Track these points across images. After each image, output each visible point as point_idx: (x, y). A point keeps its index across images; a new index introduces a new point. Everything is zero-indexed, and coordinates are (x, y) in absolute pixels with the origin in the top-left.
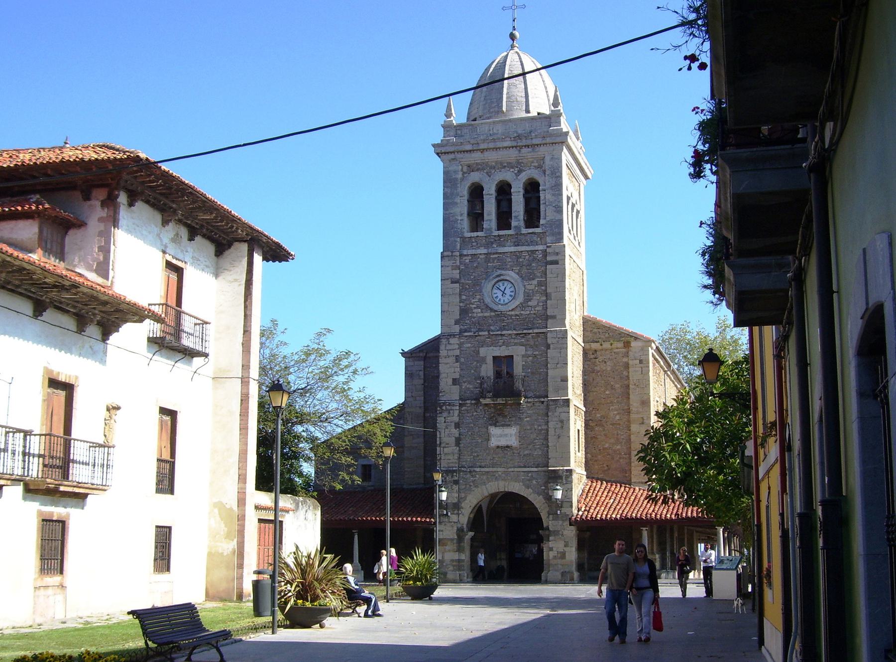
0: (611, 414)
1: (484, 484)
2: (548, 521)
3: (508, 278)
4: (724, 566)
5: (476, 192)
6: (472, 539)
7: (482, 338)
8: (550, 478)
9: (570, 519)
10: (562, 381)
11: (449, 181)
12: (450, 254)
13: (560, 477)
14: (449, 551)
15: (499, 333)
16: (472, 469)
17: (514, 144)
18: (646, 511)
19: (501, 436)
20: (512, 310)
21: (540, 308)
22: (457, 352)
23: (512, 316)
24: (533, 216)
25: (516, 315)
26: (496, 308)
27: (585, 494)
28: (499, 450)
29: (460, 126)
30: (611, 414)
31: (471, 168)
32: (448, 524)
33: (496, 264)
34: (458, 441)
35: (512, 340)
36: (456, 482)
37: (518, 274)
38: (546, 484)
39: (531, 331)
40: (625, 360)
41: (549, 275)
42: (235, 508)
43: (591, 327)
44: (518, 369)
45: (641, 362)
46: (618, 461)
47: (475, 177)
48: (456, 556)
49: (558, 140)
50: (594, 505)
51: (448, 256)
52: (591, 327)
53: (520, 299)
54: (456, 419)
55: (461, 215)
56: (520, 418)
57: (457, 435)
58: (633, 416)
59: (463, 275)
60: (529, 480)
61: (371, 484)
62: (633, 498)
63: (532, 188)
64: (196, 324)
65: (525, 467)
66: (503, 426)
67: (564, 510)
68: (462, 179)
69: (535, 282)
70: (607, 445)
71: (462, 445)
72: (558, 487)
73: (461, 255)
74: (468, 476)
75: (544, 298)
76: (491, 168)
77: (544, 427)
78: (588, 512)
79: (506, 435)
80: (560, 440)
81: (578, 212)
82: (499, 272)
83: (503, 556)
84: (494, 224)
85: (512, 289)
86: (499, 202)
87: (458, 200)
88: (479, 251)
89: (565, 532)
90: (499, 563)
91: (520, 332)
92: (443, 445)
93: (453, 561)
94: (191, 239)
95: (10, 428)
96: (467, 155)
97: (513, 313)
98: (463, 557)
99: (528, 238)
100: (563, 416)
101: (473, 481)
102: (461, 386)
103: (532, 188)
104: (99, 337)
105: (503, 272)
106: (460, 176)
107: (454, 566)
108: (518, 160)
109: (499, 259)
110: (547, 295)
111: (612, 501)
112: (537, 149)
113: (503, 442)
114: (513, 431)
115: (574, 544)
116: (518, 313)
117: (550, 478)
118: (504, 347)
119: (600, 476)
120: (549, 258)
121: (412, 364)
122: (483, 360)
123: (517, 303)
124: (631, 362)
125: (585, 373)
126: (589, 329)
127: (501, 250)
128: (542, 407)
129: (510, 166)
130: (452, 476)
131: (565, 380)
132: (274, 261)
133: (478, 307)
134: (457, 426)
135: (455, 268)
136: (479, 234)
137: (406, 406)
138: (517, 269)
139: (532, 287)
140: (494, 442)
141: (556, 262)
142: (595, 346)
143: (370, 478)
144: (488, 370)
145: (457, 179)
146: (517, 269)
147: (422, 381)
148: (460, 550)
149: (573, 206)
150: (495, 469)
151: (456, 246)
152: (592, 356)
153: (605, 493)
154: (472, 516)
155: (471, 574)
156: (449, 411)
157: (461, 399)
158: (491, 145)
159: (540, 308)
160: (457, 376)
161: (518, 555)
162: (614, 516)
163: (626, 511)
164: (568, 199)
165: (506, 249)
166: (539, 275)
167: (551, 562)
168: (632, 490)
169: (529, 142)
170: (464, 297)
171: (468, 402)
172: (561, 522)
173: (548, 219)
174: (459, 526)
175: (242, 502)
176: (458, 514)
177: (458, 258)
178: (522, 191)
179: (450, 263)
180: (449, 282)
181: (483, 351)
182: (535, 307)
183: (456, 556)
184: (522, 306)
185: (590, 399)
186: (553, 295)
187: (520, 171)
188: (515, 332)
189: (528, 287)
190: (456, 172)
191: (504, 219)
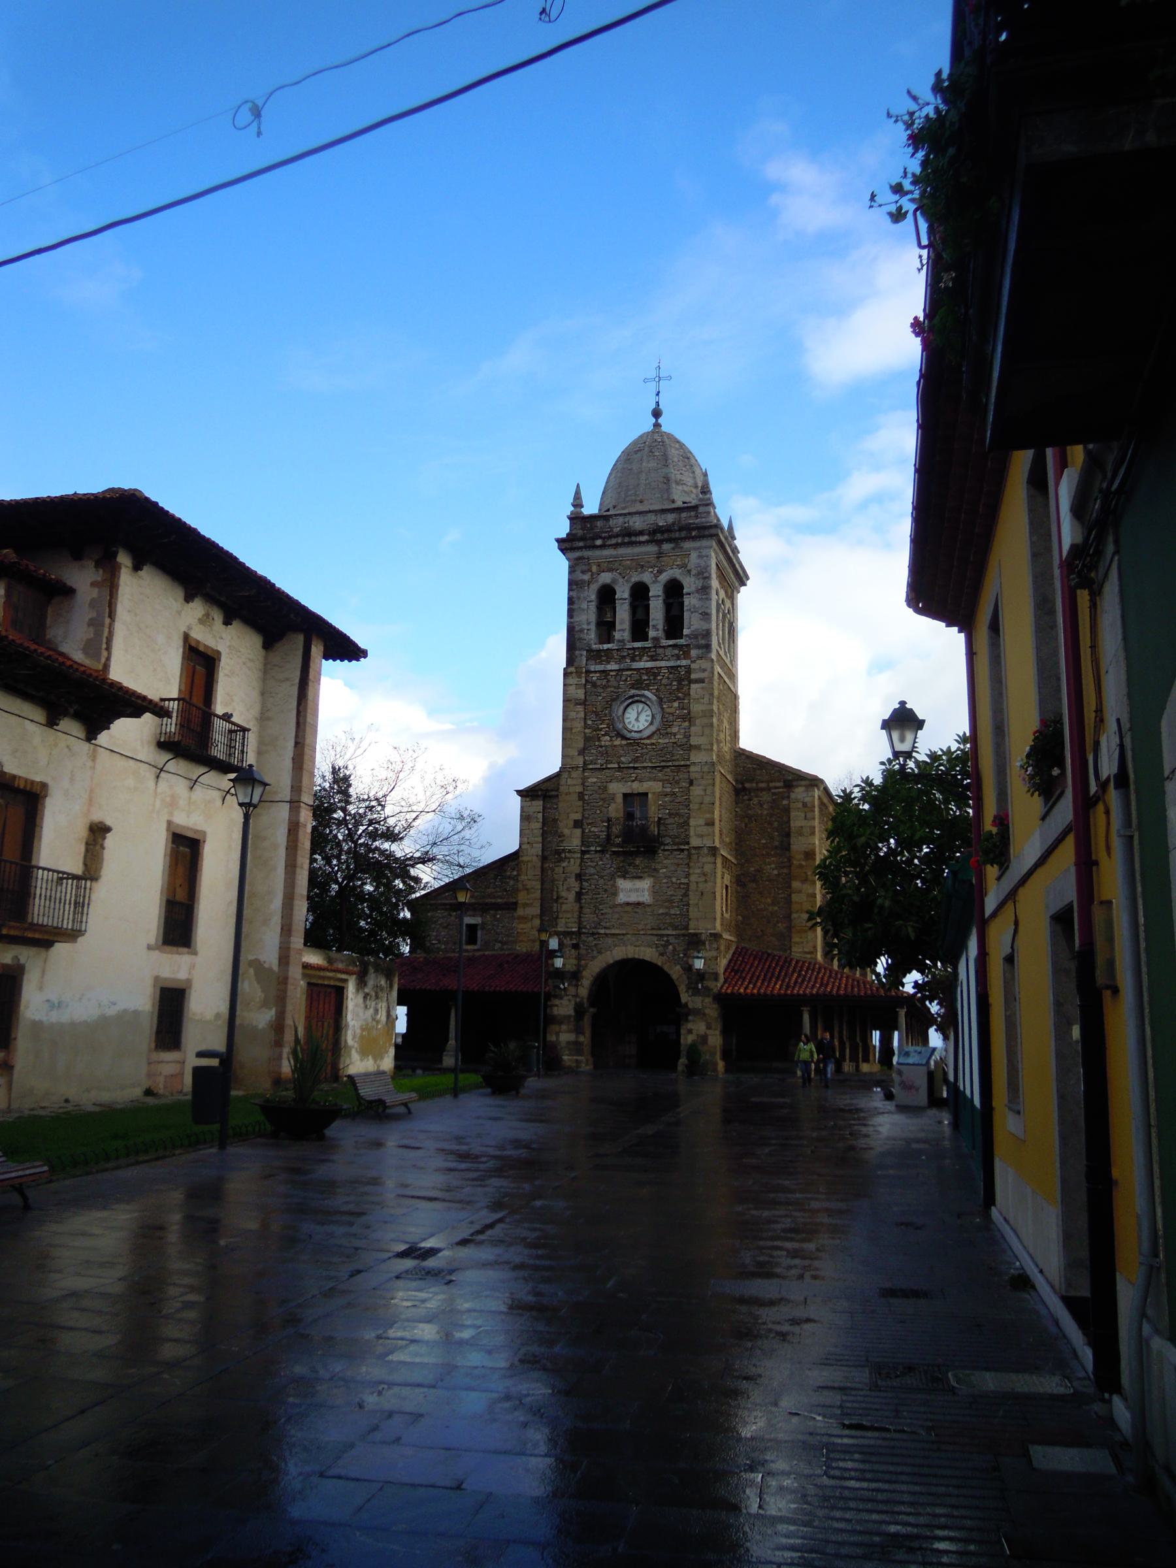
4: (910, 1061)
19: (631, 890)
20: (648, 738)
26: (629, 735)
28: (629, 908)
29: (592, 518)
34: (579, 895)
42: (275, 968)
44: (654, 812)
47: (606, 578)
48: (571, 1037)
55: (589, 624)
63: (674, 590)
64: (231, 731)
79: (637, 890)
82: (633, 692)
84: (627, 635)
86: (634, 609)
88: (609, 667)
93: (568, 1043)
94: (227, 622)
95: (64, 873)
98: (581, 1039)
103: (674, 590)
104: (82, 735)
113: (633, 898)
114: (646, 884)
120: (693, 676)
127: (636, 665)
132: (342, 660)
140: (622, 898)
141: (702, 681)
144: (616, 810)
147: (539, 825)
148: (578, 1031)
149: (724, 616)
160: (578, 817)
162: (808, 991)
164: (718, 605)
165: (641, 665)
175: (284, 957)
183: (571, 1037)
187: (660, 572)
191: (639, 629)
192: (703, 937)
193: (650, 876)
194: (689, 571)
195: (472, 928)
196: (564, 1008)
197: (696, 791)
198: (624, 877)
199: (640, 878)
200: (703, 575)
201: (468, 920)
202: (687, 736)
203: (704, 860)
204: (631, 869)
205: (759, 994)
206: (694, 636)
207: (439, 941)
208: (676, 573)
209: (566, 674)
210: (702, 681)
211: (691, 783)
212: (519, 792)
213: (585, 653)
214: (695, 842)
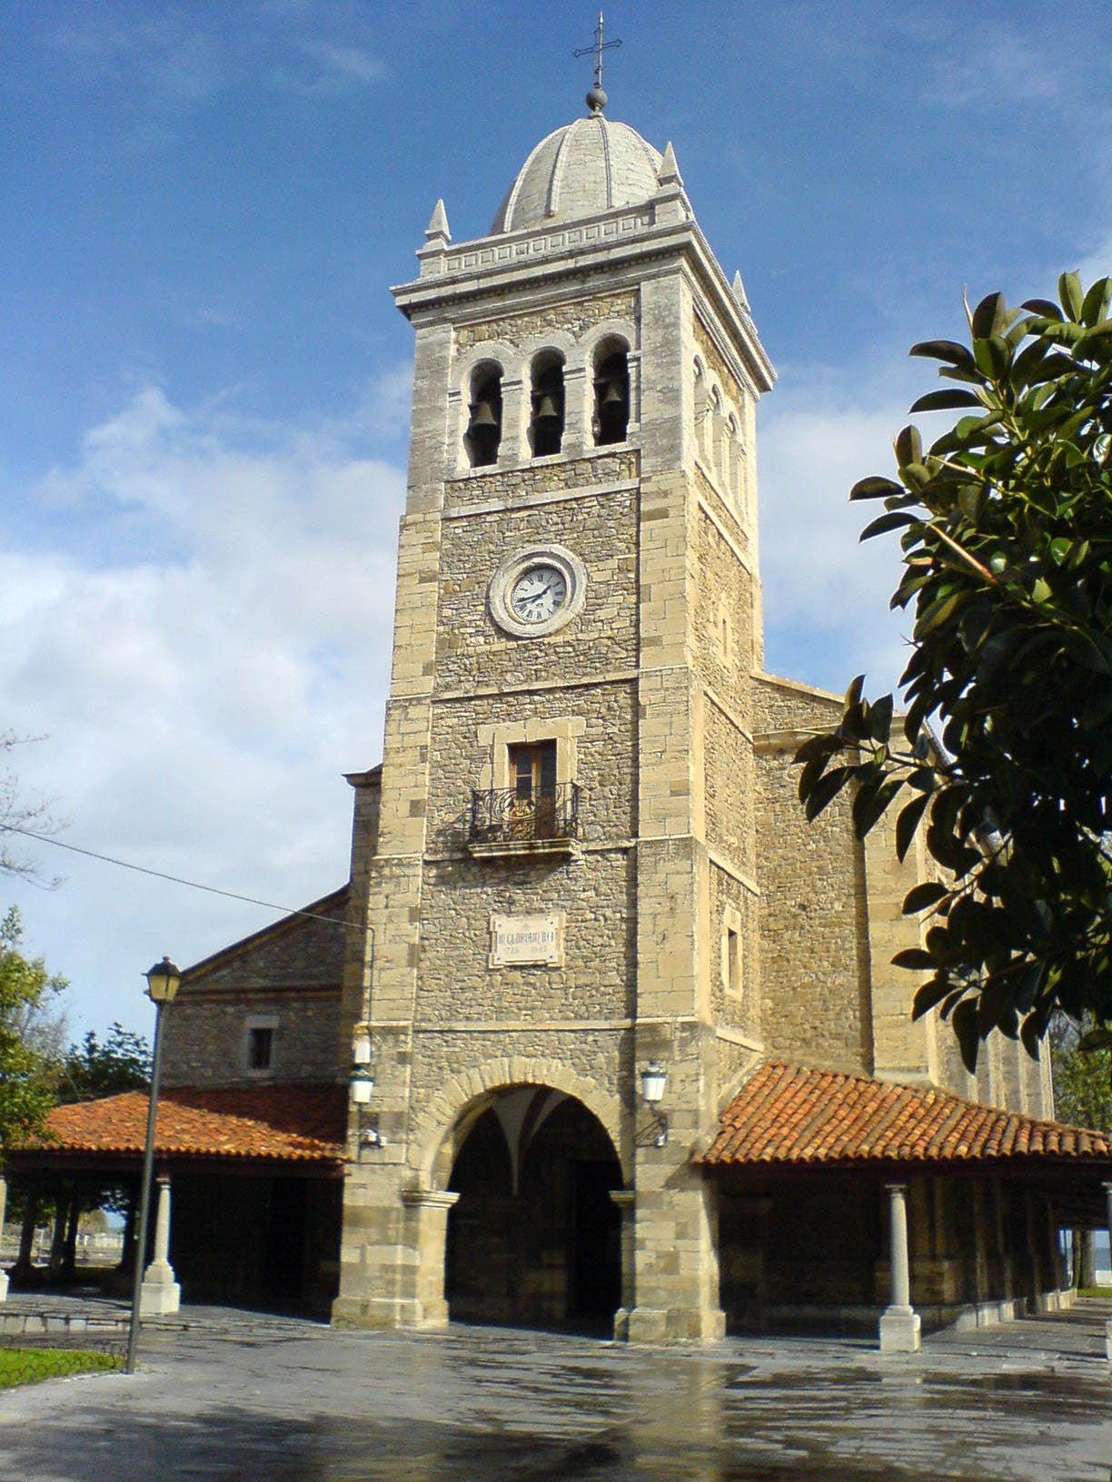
6: (454, 1214)
15: (525, 687)
19: (520, 938)
20: (557, 632)
25: (568, 644)
28: (517, 976)
39: (599, 679)
44: (568, 769)
51: (415, 523)
63: (612, 362)
69: (613, 563)
79: (532, 938)
80: (667, 946)
82: (530, 548)
92: (378, 964)
97: (559, 639)
100: (677, 883)
103: (612, 362)
113: (525, 954)
122: (488, 754)
136: (488, 469)
137: (352, 893)
139: (605, 576)
140: (502, 955)
141: (663, 514)
143: (267, 1063)
179: (421, 539)
184: (583, 621)
189: (597, 577)
191: (546, 435)
192: (666, 1032)
195: (262, 1036)
200: (668, 324)
201: (255, 1021)
203: (670, 866)
206: (652, 429)
207: (205, 1064)
208: (621, 327)
210: (663, 514)
212: (351, 778)
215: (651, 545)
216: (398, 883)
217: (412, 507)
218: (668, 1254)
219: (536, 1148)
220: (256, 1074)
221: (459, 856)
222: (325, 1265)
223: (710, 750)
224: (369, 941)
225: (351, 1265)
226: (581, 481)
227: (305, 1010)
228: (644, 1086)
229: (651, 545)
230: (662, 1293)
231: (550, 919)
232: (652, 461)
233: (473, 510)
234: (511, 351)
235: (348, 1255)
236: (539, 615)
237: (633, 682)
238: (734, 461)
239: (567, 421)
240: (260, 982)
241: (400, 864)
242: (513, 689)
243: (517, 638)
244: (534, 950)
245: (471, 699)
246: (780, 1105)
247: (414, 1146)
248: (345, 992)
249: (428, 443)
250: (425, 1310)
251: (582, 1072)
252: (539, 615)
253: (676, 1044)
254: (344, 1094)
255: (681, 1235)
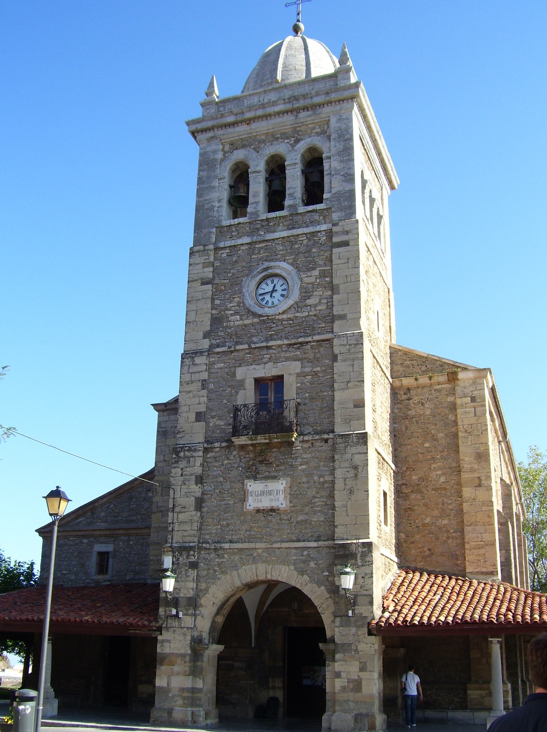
0: (433, 475)
1: (236, 568)
2: (333, 628)
3: (278, 271)
5: (241, 176)
6: (220, 657)
7: (241, 354)
8: (336, 557)
9: (369, 624)
10: (356, 406)
11: (206, 164)
12: (201, 248)
13: (353, 556)
14: (178, 674)
15: (264, 344)
16: (218, 545)
17: (288, 106)
18: (495, 610)
19: (263, 493)
20: (284, 312)
21: (322, 307)
22: (205, 375)
23: (283, 320)
24: (314, 192)
25: (290, 319)
26: (260, 311)
27: (396, 588)
30: (433, 475)
31: (234, 146)
32: (178, 631)
33: (263, 254)
34: (199, 503)
35: (283, 354)
36: (194, 565)
37: (292, 264)
38: (330, 567)
39: (309, 339)
40: (450, 399)
41: (335, 261)
43: (403, 362)
44: (290, 392)
45: (473, 399)
46: (445, 541)
47: (239, 155)
48: (188, 682)
49: (347, 94)
50: (410, 603)
51: (198, 251)
52: (403, 362)
53: (295, 296)
54: (198, 470)
55: (220, 201)
56: (292, 466)
57: (198, 494)
58: (465, 476)
59: (217, 272)
60: (304, 562)
61: (107, 577)
62: (470, 593)
63: (314, 164)
65: (298, 541)
66: (267, 478)
67: (359, 609)
68: (222, 160)
69: (316, 273)
70: (428, 520)
71: (205, 510)
72: (348, 570)
73: (217, 249)
74: (213, 555)
75: (329, 293)
76: (260, 142)
77: (328, 478)
78: (400, 612)
79: (270, 493)
80: (353, 497)
81: (380, 217)
82: (266, 264)
83: (278, 683)
85: (284, 287)
86: (269, 181)
87: (216, 183)
89: (361, 647)
90: (271, 694)
91: (293, 341)
92: (177, 509)
93: (183, 690)
96: (230, 130)
98: (199, 684)
99: (307, 218)
100: (357, 459)
101: (219, 565)
102: (207, 424)
105: (272, 264)
106: (220, 156)
107: (184, 698)
108: (295, 128)
109: (266, 249)
110: (333, 289)
111: (437, 597)
112: (320, 111)
113: (265, 503)
114: (280, 485)
115: (377, 665)
116: (290, 316)
117: (336, 557)
118: (270, 364)
119: (420, 565)
120: (335, 240)
121: (166, 418)
123: (290, 302)
124: (458, 401)
125: (394, 419)
126: (399, 362)
128: (326, 447)
129: (285, 136)
130: (188, 557)
131: (360, 404)
133: (236, 313)
134: (200, 480)
135: (206, 265)
136: (242, 220)
137: (156, 473)
138: (291, 258)
139: (312, 280)
140: (252, 504)
141: (346, 244)
142: (407, 382)
143: (107, 571)
144: (247, 396)
145: (215, 160)
146: (291, 258)
148: (195, 672)
150: (252, 545)
151: (210, 237)
152: (404, 397)
153: (427, 587)
154: (220, 619)
155: (214, 712)
156: (188, 459)
157: (207, 442)
158: (260, 113)
159: (322, 307)
161: (307, 682)
162: (442, 618)
163: (462, 611)
165: (277, 235)
166: (321, 262)
167: (339, 697)
168: (467, 584)
169: (308, 102)
170: (217, 302)
171: (217, 445)
172: (353, 630)
173: (334, 191)
174: (196, 634)
176: (195, 615)
177: (212, 253)
178: (299, 167)
179: (202, 259)
180: (199, 283)
181: (240, 373)
182: (316, 305)
183: (188, 682)
184: (297, 306)
185: (403, 455)
186: (341, 287)
187: (297, 141)
188: (286, 342)
189: (307, 280)
190: (215, 152)
191: (276, 200)
193: (285, 475)
194: (329, 137)
195: (103, 556)
196: (173, 642)
197: (339, 367)
198: (255, 479)
199: (275, 478)
201: (99, 548)
202: (331, 307)
204: (262, 468)
205: (421, 623)
206: (338, 196)
209: (192, 253)
211: (335, 358)
213: (214, 230)
214: (339, 429)
215: (339, 261)
216: (189, 462)
217: (196, 242)
218: (354, 681)
219: (266, 618)
220: (101, 577)
221: (224, 444)
222: (143, 689)
223: (373, 385)
224: (172, 496)
225: (161, 688)
226: (297, 226)
227: (129, 540)
228: (340, 580)
229: (339, 261)
230: (352, 705)
231: (280, 482)
232: (339, 214)
233: (233, 243)
234: (255, 155)
235: (160, 682)
236: (273, 303)
237: (329, 341)
238: (379, 223)
239: (288, 192)
240: (103, 525)
241: (190, 450)
242: (257, 345)
243: (260, 316)
244: (271, 500)
245: (232, 352)
246: (416, 593)
247: (199, 617)
248: (152, 530)
249: (206, 206)
250: (206, 714)
251: (302, 572)
252: (273, 303)
253: (359, 555)
254: (157, 586)
255: (363, 669)
